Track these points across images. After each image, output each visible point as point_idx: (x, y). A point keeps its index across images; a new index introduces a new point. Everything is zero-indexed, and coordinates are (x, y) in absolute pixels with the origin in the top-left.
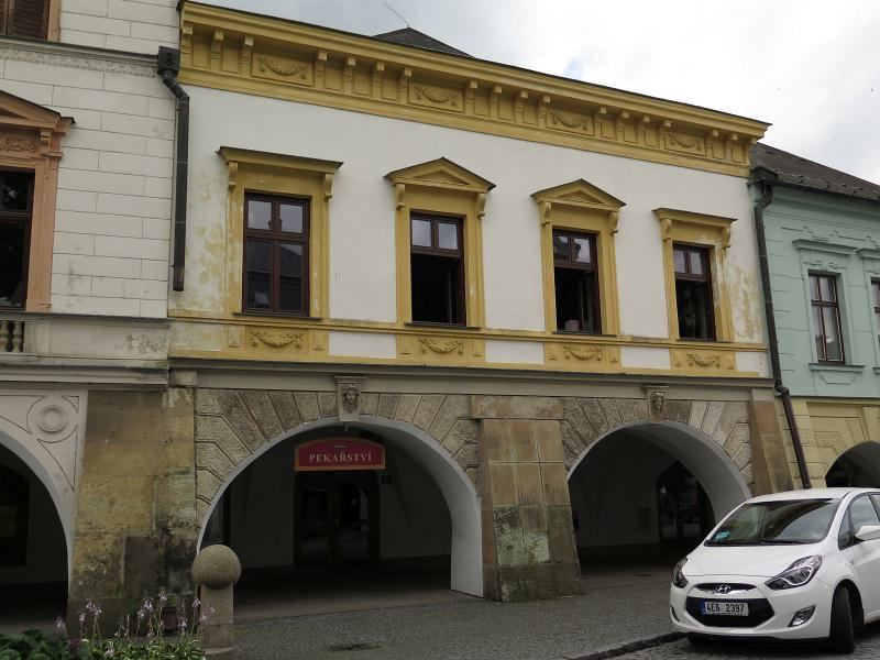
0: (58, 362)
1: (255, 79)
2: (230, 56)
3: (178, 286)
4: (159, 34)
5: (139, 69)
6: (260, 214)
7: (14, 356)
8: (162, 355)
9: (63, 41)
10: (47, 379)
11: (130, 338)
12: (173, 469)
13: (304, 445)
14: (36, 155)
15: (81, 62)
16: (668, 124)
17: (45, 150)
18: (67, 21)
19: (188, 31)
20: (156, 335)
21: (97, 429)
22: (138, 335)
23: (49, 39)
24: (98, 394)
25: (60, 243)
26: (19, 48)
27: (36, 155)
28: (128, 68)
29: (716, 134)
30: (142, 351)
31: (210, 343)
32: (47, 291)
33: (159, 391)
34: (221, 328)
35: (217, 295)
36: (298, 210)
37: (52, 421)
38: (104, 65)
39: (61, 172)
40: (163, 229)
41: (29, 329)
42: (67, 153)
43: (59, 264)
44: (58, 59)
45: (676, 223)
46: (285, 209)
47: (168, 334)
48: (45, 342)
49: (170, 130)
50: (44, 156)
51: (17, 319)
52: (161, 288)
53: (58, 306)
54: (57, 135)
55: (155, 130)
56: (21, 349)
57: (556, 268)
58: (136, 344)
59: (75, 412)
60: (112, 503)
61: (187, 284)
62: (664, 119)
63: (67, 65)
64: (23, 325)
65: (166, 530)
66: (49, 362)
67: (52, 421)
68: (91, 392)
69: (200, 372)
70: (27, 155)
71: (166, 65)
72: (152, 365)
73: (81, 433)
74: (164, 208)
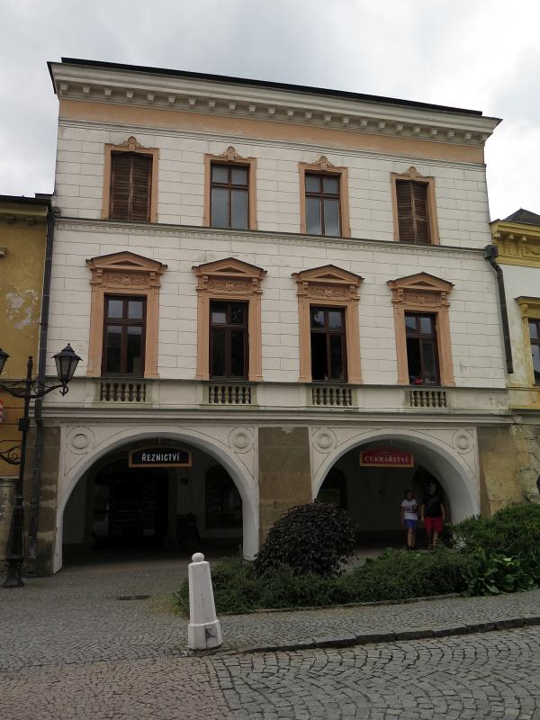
0: (462, 412)
1: (525, 258)
2: (512, 247)
3: (510, 371)
4: (483, 241)
5: (476, 257)
6: (116, 308)
7: (443, 410)
8: (506, 408)
9: (442, 244)
10: (458, 421)
11: (491, 399)
12: (522, 468)
13: (361, 459)
14: (146, 287)
15: (451, 255)
16: (524, 239)
17: (153, 284)
18: (442, 234)
19: (497, 235)
20: (502, 397)
21: (483, 447)
22: (495, 397)
23: (152, 221)
24: (482, 429)
25: (455, 350)
26: (137, 228)
27: (146, 287)
28: (472, 257)
29: (512, 237)
30: (497, 405)
31: (524, 401)
32: (451, 377)
33: (507, 427)
34: (527, 392)
35: (524, 376)
36: (338, 314)
37: (241, 441)
38: (461, 256)
39: (450, 314)
40: (497, 341)
41: (448, 395)
42: (264, 291)
43: (455, 361)
44: (441, 254)
45: (531, 306)
46: (131, 304)
47: (504, 396)
48: (456, 402)
49: (494, 288)
50: (255, 292)
51: (437, 390)
52: (501, 372)
53: (163, 375)
54: (158, 274)
55: (487, 289)
56: (445, 405)
57: (408, 340)
58: (494, 402)
59: (472, 438)
60: (501, 485)
61: (514, 370)
62: (509, 233)
63: (92, 232)
64: (444, 393)
65: (528, 500)
66: (458, 412)
67: (241, 441)
68: (478, 428)
69: (523, 416)
70: (142, 287)
71: (490, 255)
72: (503, 413)
73: (476, 449)
74: (496, 329)
